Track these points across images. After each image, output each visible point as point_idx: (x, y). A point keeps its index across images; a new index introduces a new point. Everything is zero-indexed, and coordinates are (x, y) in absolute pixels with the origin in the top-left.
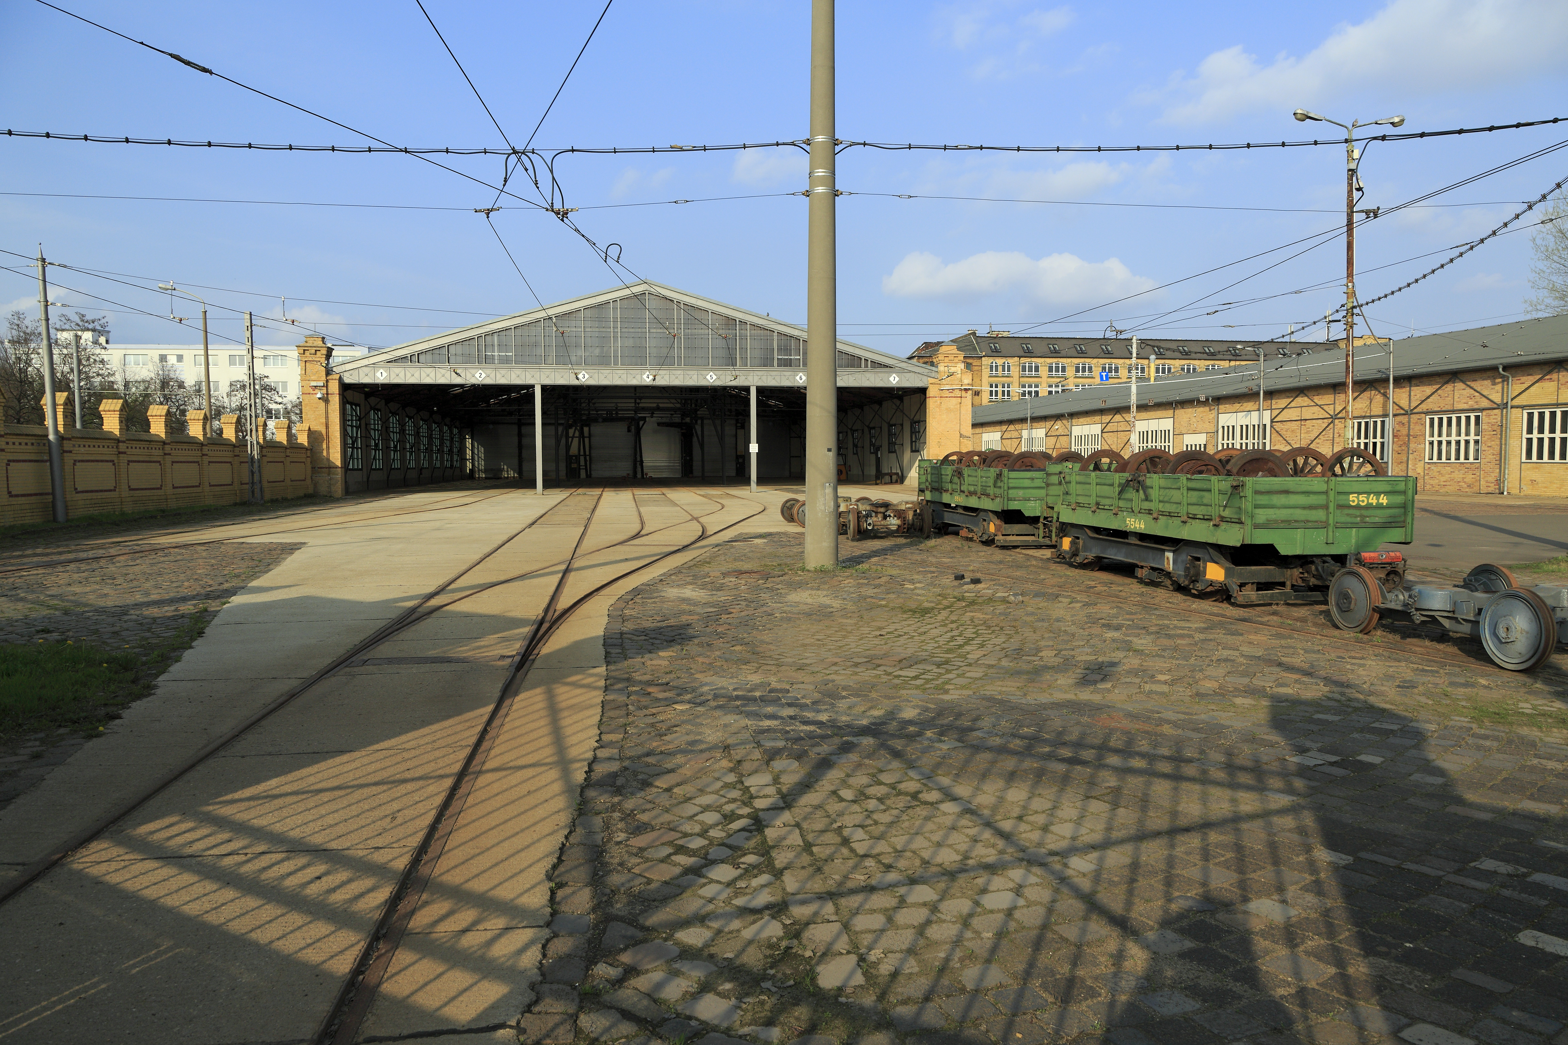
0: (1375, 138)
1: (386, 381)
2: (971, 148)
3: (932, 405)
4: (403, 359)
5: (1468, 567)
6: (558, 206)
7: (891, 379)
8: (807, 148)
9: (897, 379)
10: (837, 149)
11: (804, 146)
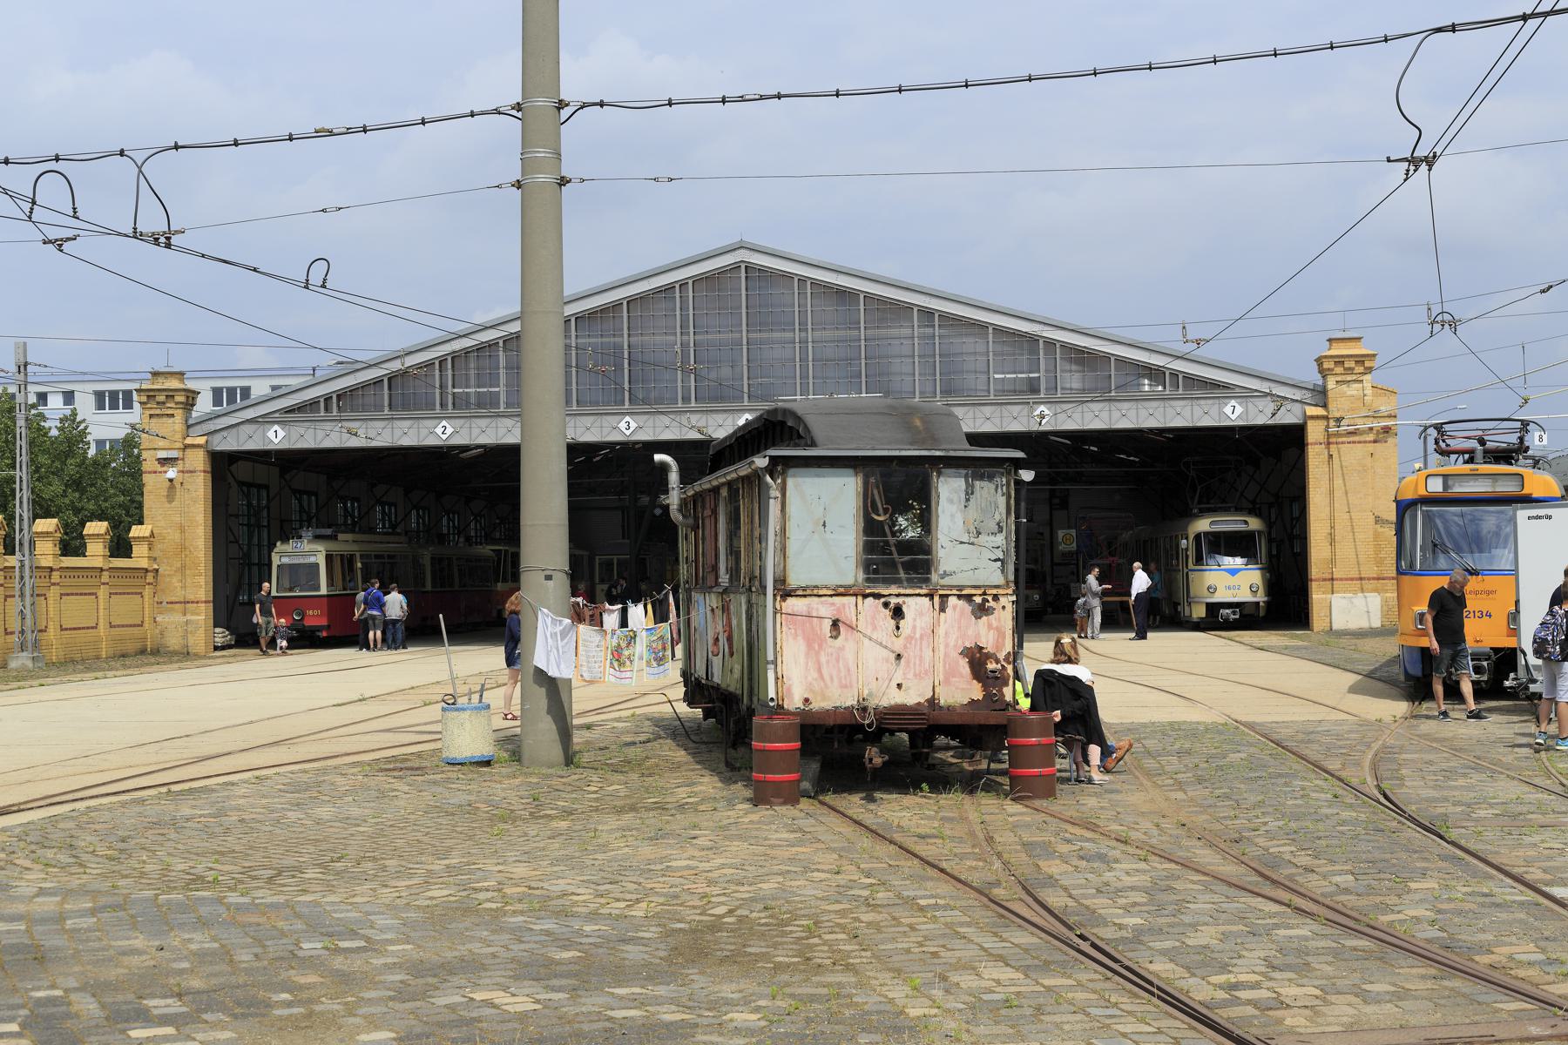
0: (1439, 30)
1: (285, 446)
2: (762, 98)
3: (1315, 458)
4: (312, 405)
5: (904, 609)
6: (152, 222)
7: (1228, 410)
8: (519, 115)
10: (565, 113)
11: (514, 112)
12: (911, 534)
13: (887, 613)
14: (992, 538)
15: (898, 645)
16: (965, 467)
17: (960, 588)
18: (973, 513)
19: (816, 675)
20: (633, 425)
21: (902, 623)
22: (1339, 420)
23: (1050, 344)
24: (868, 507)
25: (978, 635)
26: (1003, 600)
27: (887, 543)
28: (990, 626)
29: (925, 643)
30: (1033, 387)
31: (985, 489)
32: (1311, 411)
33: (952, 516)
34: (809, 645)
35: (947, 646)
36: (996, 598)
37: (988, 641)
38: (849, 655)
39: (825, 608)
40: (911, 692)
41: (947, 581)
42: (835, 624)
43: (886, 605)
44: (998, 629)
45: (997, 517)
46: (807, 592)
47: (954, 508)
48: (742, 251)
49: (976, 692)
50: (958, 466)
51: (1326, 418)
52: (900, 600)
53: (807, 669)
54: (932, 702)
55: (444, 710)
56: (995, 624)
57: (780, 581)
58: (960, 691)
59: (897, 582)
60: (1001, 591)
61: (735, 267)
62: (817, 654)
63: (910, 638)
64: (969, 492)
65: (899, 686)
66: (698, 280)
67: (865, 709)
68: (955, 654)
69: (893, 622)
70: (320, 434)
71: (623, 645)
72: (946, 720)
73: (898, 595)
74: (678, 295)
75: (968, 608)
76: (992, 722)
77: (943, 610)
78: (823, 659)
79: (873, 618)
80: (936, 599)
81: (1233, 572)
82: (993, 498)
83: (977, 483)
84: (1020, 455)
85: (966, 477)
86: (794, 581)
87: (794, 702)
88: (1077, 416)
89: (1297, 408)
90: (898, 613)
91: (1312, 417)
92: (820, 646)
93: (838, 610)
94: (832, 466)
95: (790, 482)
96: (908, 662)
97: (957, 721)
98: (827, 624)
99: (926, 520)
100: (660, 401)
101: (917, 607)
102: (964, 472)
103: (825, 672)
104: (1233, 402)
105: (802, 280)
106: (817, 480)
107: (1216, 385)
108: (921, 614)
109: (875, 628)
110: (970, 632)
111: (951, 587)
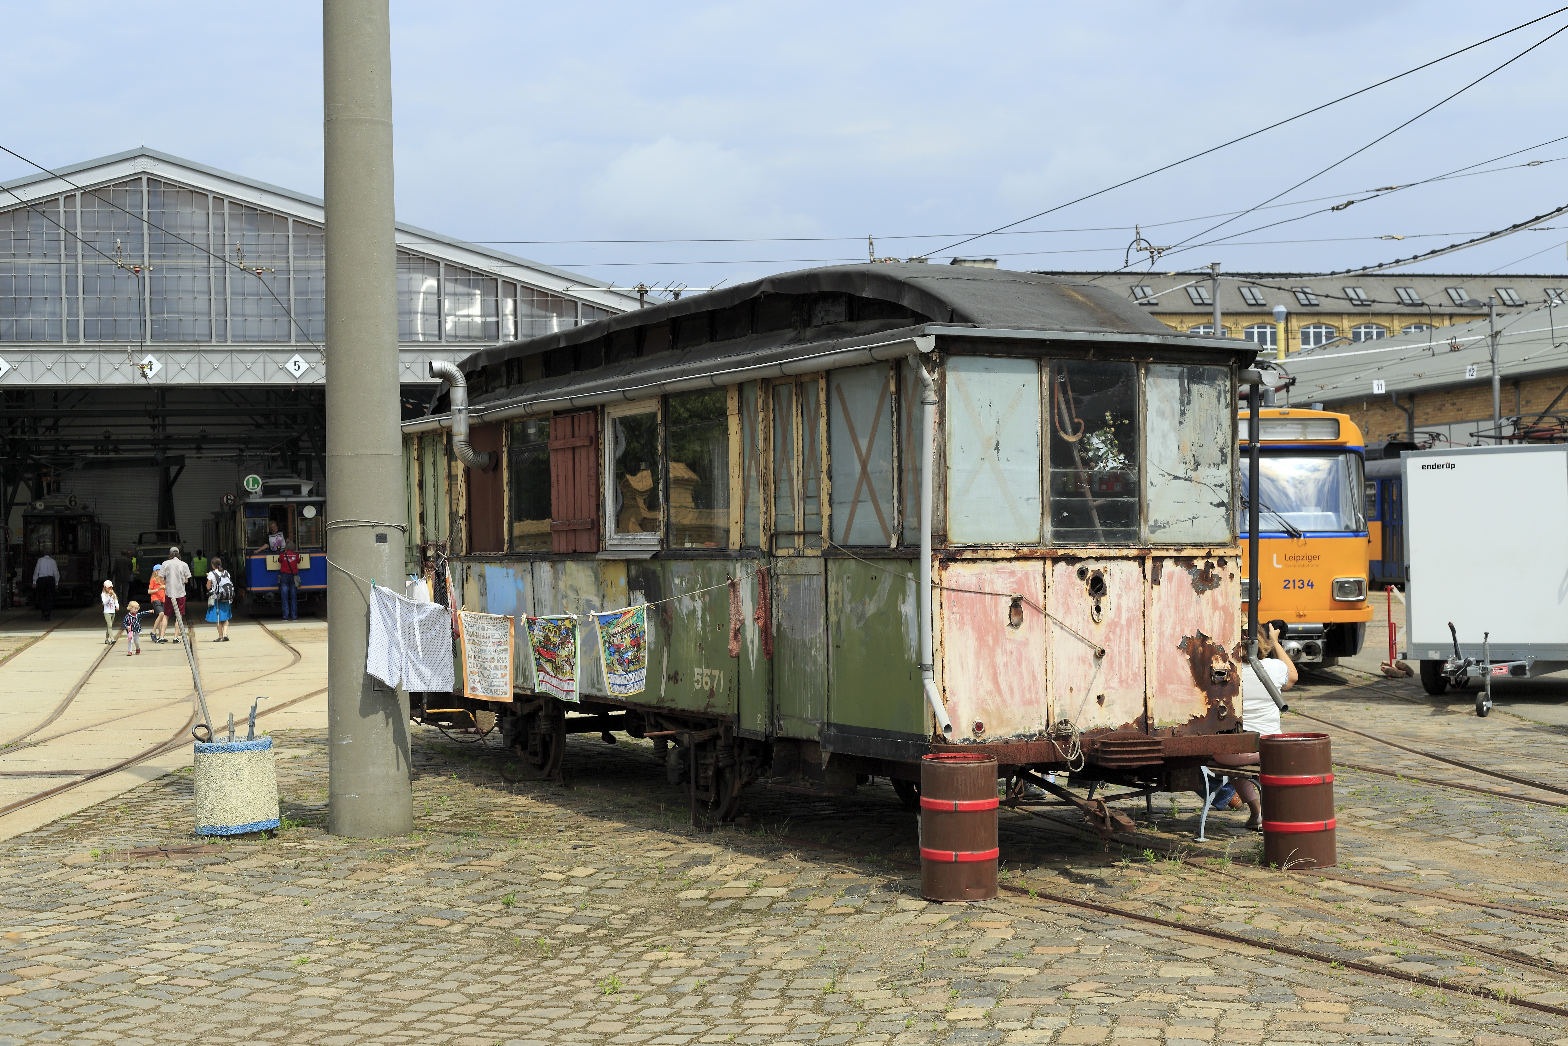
5: (1107, 580)
12: (1113, 463)
13: (1084, 586)
14: (1214, 471)
15: (1098, 635)
16: (1179, 362)
17: (1179, 547)
18: (1190, 433)
19: (990, 686)
21: (1103, 600)
25: (1200, 619)
26: (1231, 565)
27: (1077, 476)
28: (1215, 606)
29: (1133, 631)
33: (1164, 436)
34: (981, 640)
35: (1161, 635)
36: (1222, 562)
37: (1213, 630)
38: (1035, 653)
39: (1001, 579)
41: (1160, 537)
42: (1016, 605)
44: (1224, 609)
45: (1220, 440)
46: (979, 553)
48: (143, 160)
50: (1171, 361)
52: (1100, 566)
53: (978, 677)
54: (1144, 721)
55: (197, 750)
56: (1221, 601)
57: (940, 536)
58: (1179, 705)
59: (1092, 537)
60: (1230, 552)
61: (136, 179)
62: (992, 651)
63: (1114, 625)
64: (1185, 400)
65: (1100, 699)
66: (88, 192)
67: (1066, 738)
68: (1171, 648)
69: (1091, 600)
71: (556, 640)
73: (1097, 559)
74: (62, 209)
75: (1188, 578)
77: (1156, 581)
78: (1000, 660)
79: (1066, 594)
80: (1149, 564)
83: (1195, 388)
85: (1181, 378)
86: (957, 537)
87: (962, 733)
90: (1097, 586)
92: (996, 640)
93: (1020, 582)
94: (1009, 355)
95: (951, 378)
96: (1111, 663)
98: (1005, 604)
99: (1128, 440)
100: (37, 337)
102: (1177, 369)
103: (1002, 680)
105: (219, 199)
106: (986, 376)
108: (1128, 588)
109: (1068, 611)
110: (1190, 615)
111: (1166, 546)
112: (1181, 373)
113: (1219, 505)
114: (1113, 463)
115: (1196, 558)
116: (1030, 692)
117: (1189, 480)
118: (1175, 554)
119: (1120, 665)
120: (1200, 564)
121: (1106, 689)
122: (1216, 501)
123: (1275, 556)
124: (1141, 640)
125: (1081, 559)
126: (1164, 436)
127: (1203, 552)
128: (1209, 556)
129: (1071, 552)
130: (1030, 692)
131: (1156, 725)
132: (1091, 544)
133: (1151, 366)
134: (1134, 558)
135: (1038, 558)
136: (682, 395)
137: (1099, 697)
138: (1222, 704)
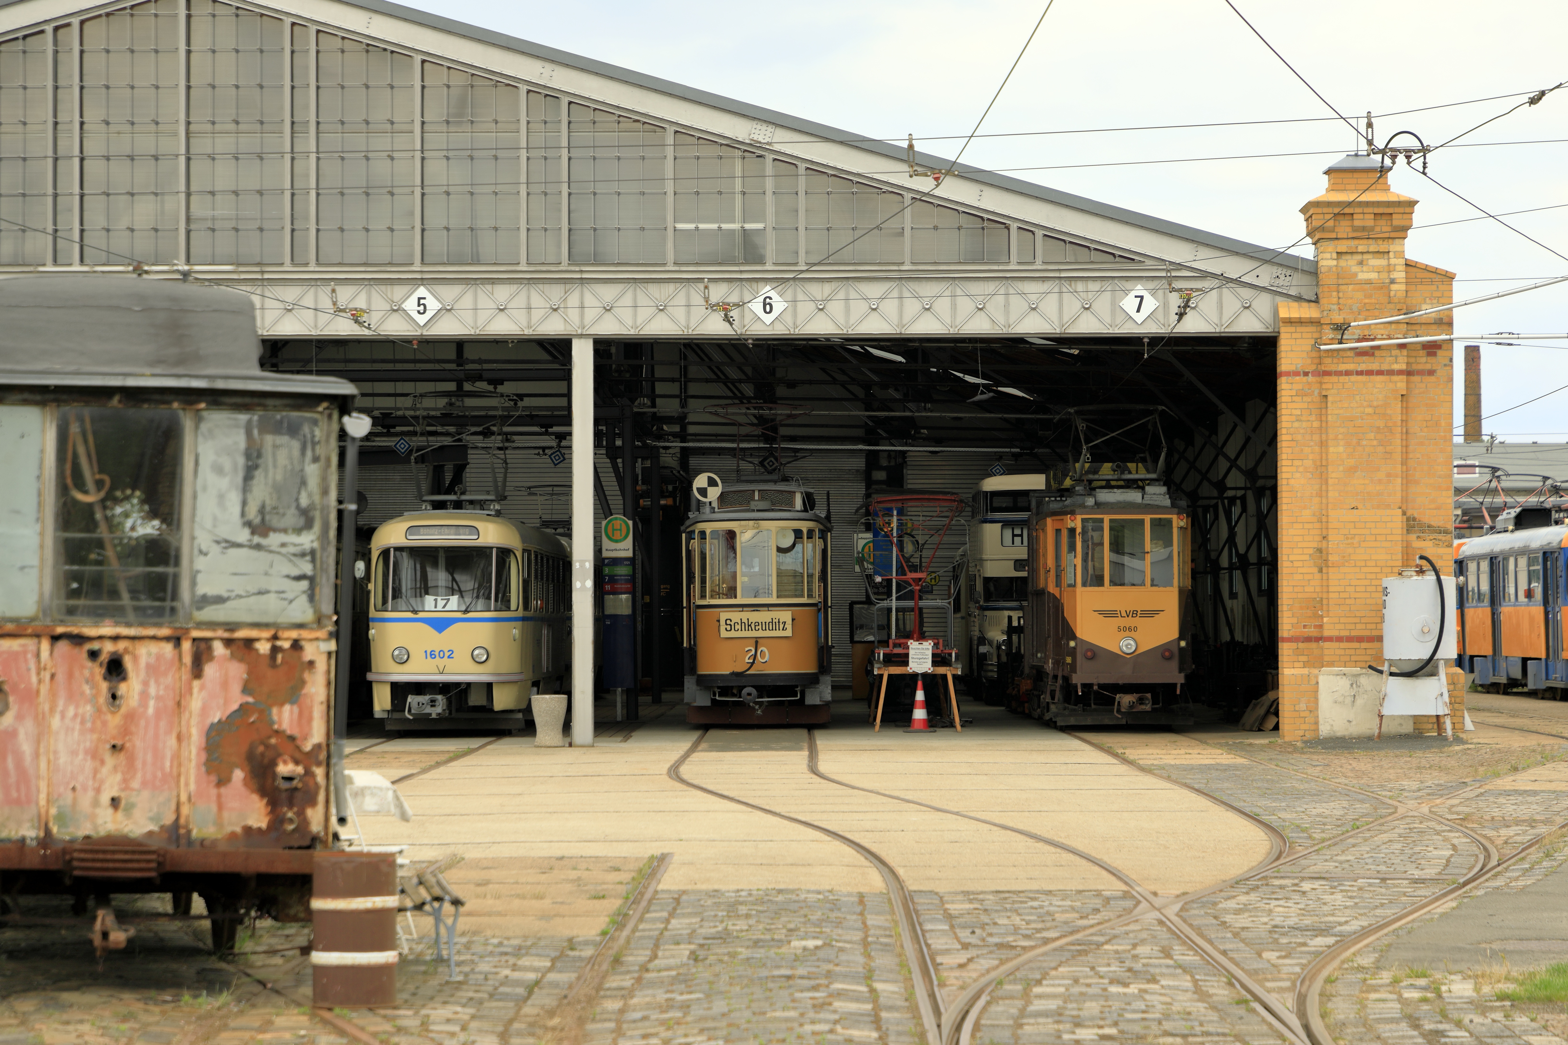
1: (780, 330)
5: (128, 662)
7: (1129, 303)
9: (1150, 304)
12: (150, 528)
13: (98, 671)
14: (292, 538)
17: (231, 627)
20: (433, 305)
22: (1341, 328)
23: (788, 162)
24: (69, 475)
30: (748, 250)
31: (281, 452)
32: (1289, 310)
33: (221, 497)
40: (137, 813)
41: (209, 613)
43: (93, 655)
47: (224, 483)
49: (256, 814)
51: (1316, 323)
52: (121, 645)
54: (47, 840)
59: (117, 614)
60: (305, 634)
69: (104, 686)
70: (859, 308)
72: (195, 863)
76: (281, 868)
77: (197, 671)
80: (186, 645)
81: (440, 625)
82: (309, 467)
83: (269, 439)
84: (345, 388)
88: (890, 307)
89: (1263, 304)
90: (115, 668)
91: (1290, 322)
97: (216, 865)
101: (150, 659)
102: (243, 417)
104: (1139, 289)
107: (1127, 258)
111: (212, 625)
112: (249, 422)
113: (299, 578)
114: (150, 528)
115: (258, 640)
116: (18, 790)
117: (258, 547)
118: (226, 635)
119: (144, 763)
120: (264, 647)
121: (123, 790)
122: (296, 572)
123: (1178, 692)
124: (174, 735)
125: (90, 639)
126: (221, 497)
127: (267, 634)
128: (275, 637)
129: (75, 630)
130: (18, 790)
131: (195, 833)
132: (107, 621)
133: (205, 414)
134: (167, 639)
135: (31, 636)
136: (1022, 686)
137: (113, 799)
138: (290, 815)
